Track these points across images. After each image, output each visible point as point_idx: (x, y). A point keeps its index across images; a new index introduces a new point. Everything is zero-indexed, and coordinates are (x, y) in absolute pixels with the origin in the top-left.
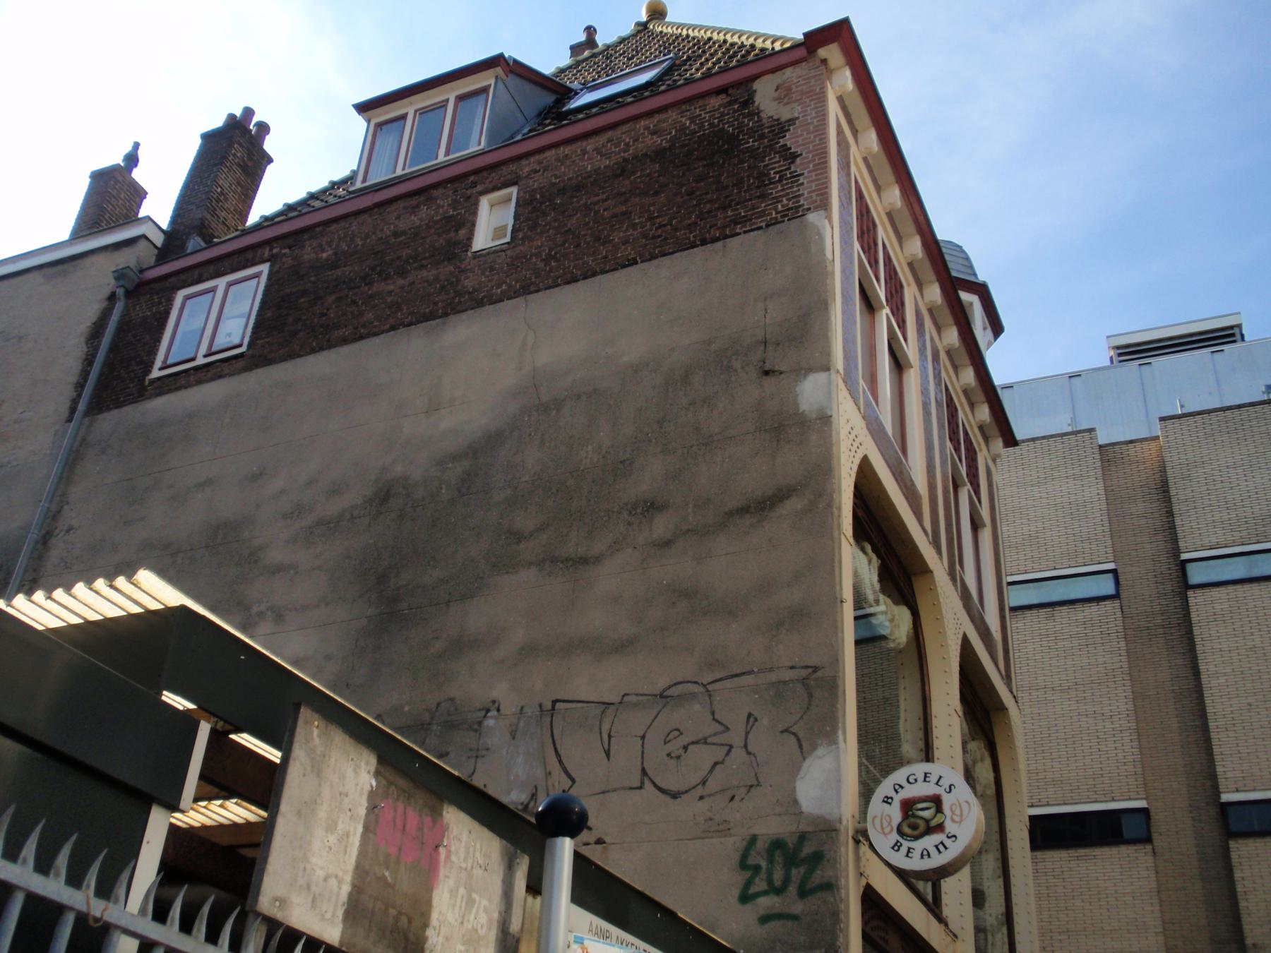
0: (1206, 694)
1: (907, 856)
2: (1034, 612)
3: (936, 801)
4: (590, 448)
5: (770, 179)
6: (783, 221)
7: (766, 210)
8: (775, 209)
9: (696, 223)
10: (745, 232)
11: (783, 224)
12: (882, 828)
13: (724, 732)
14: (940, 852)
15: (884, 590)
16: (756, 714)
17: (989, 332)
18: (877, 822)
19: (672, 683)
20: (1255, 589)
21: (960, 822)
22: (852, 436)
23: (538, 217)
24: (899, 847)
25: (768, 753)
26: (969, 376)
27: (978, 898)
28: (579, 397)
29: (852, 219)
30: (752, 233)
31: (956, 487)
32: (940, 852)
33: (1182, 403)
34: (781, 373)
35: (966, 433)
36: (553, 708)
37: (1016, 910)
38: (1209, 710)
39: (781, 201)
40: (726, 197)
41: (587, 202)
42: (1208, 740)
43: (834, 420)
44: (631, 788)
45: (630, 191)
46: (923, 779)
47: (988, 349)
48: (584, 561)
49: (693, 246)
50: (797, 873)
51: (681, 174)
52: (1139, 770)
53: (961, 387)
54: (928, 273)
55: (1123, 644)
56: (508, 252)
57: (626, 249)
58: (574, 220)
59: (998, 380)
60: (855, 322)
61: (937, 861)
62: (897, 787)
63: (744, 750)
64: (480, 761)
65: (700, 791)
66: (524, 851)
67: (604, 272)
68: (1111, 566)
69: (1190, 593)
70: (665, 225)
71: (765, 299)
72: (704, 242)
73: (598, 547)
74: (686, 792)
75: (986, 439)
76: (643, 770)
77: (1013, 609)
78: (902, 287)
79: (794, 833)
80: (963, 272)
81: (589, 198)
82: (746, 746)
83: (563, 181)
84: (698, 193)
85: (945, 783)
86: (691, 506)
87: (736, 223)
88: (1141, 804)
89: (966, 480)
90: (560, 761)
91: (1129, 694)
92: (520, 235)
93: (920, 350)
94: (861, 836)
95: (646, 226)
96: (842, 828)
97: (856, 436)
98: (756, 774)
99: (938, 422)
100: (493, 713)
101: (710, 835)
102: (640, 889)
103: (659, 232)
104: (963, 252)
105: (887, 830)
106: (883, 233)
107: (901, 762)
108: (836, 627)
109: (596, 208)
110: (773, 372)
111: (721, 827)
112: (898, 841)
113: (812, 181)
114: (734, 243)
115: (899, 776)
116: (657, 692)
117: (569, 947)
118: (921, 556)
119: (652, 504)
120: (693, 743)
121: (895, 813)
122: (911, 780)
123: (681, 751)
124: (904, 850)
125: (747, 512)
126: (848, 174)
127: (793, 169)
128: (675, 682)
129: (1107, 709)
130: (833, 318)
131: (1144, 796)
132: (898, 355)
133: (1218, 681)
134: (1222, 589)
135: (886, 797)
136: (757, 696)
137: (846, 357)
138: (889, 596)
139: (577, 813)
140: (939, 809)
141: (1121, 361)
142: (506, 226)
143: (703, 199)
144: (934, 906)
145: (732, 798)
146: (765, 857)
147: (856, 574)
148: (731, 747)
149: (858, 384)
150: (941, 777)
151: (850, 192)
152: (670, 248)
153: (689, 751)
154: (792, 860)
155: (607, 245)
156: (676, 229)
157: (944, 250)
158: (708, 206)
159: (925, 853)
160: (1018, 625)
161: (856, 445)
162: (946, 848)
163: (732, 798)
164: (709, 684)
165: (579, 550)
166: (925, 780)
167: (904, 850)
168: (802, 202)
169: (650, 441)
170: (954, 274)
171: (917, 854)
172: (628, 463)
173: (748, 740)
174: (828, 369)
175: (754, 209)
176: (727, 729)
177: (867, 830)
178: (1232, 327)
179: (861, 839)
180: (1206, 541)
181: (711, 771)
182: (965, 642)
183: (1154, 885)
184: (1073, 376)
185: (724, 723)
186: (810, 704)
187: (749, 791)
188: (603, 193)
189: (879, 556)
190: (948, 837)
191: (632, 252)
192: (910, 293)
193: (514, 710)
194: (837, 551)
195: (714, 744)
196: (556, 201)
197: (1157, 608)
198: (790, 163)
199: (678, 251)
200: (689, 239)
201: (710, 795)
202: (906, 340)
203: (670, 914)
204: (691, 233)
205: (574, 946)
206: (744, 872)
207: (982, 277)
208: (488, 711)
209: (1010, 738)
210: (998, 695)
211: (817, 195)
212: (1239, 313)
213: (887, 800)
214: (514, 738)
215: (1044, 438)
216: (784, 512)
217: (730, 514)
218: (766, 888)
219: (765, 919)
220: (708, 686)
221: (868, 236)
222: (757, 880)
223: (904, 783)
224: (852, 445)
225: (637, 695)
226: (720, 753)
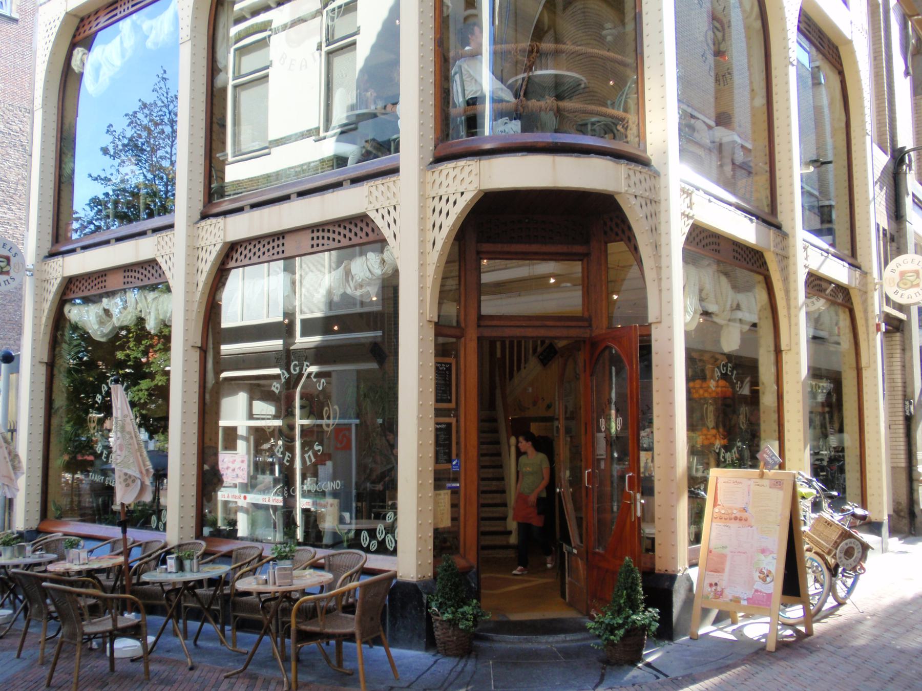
140: (8, 264)
167: (899, 294)
223: (902, 264)
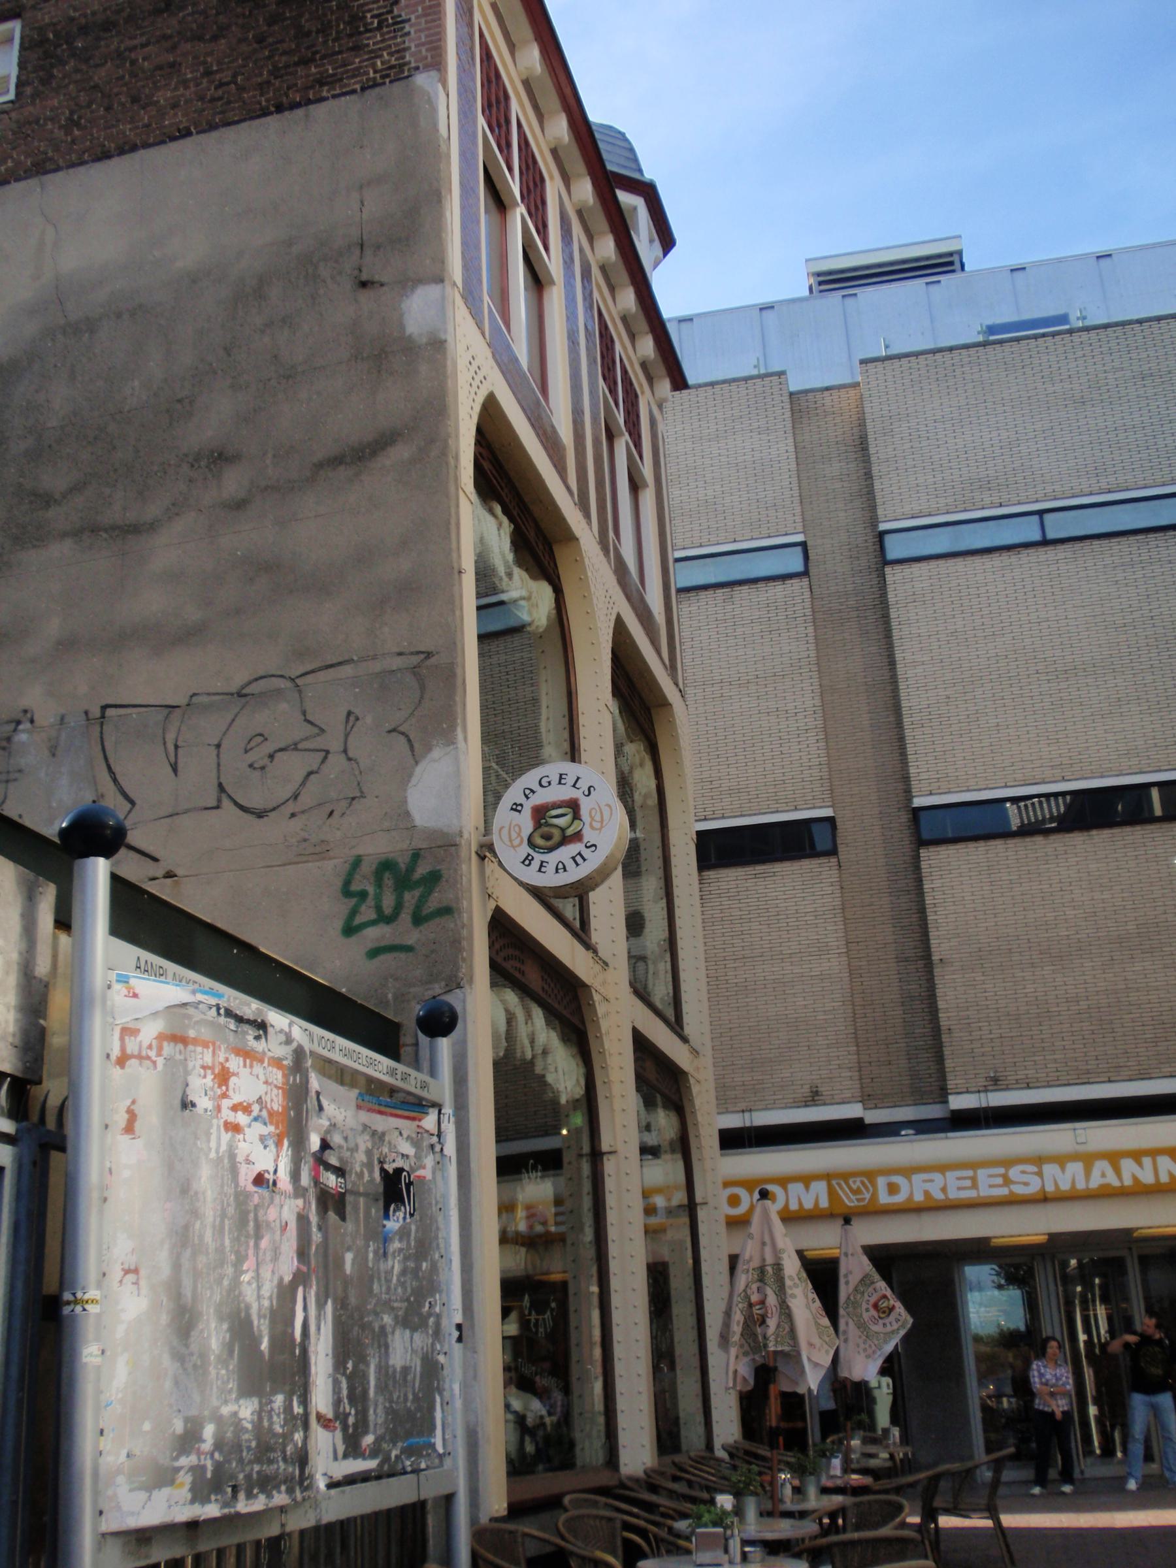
0: (902, 686)
1: (540, 870)
2: (710, 592)
3: (573, 806)
4: (136, 383)
5: (365, 25)
6: (384, 83)
7: (361, 67)
8: (374, 66)
9: (268, 82)
10: (334, 97)
11: (383, 88)
12: (511, 841)
13: (318, 735)
14: (577, 865)
15: (519, 562)
16: (357, 711)
17: (657, 248)
18: (505, 832)
19: (252, 678)
20: (959, 564)
21: (600, 829)
22: (474, 367)
23: (52, 66)
24: (530, 861)
25: (373, 758)
26: (628, 299)
27: (635, 924)
28: (119, 316)
29: (475, 84)
30: (343, 98)
31: (611, 437)
32: (577, 865)
33: (887, 343)
34: (382, 285)
35: (625, 371)
36: (103, 717)
37: (680, 934)
38: (904, 704)
39: (382, 56)
40: (308, 48)
41: (119, 47)
42: (901, 739)
43: (450, 345)
44: (206, 809)
45: (179, 33)
46: (557, 781)
47: (655, 267)
48: (135, 529)
49: (265, 113)
50: (410, 898)
51: (247, 13)
52: (825, 775)
53: (619, 313)
54: (577, 165)
55: (811, 630)
56: (13, 115)
57: (176, 115)
58: (102, 72)
59: (668, 310)
60: (478, 222)
61: (575, 874)
62: (527, 792)
63: (343, 755)
64: (11, 786)
65: (291, 807)
66: (50, 878)
67: (146, 145)
68: (800, 538)
69: (888, 570)
70: (228, 84)
71: (361, 187)
72: (280, 109)
73: (153, 510)
74: (274, 809)
75: (650, 379)
76: (220, 785)
77: (680, 591)
78: (542, 180)
79: (407, 850)
80: (625, 167)
81: (122, 41)
82: (345, 751)
83: (85, 16)
84: (271, 40)
85: (583, 785)
86: (270, 455)
87: (322, 84)
88: (827, 812)
89: (624, 429)
90: (115, 780)
91: (816, 687)
92: (28, 90)
93: (565, 262)
94: (486, 851)
95: (201, 83)
96: (463, 842)
97: (479, 368)
98: (359, 784)
99: (588, 355)
100: (26, 725)
101: (305, 858)
102: (209, 921)
103: (220, 92)
104: (626, 140)
105: (516, 842)
106: (519, 107)
107: (536, 761)
108: (453, 603)
109: (133, 55)
110: (373, 283)
111: (318, 849)
112: (529, 855)
113: (420, 31)
114: (319, 111)
115: (530, 779)
116: (234, 690)
117: (109, 987)
118: (564, 519)
119: (220, 455)
120: (281, 750)
121: (526, 823)
122: (544, 783)
123: (266, 761)
124: (536, 864)
125: (341, 463)
126: (470, 24)
127: (396, 12)
128: (255, 677)
129: (790, 706)
130: (448, 214)
131: (830, 804)
132: (537, 268)
133: (915, 671)
134: (923, 566)
135: (515, 804)
136: (357, 690)
137: (466, 267)
138: (527, 570)
139: (111, 827)
140: (576, 816)
141: (821, 291)
142: (8, 77)
143: (277, 49)
144: (581, 932)
145: (331, 813)
146: (372, 881)
147: (481, 541)
148: (327, 752)
149: (482, 301)
150: (578, 778)
151: (472, 49)
152: (235, 115)
153: (276, 760)
154: (404, 882)
155: (148, 109)
156: (241, 89)
157: (597, 136)
158: (284, 58)
159: (561, 866)
160: (689, 612)
161: (478, 378)
162: (584, 860)
163: (331, 813)
164: (297, 677)
165: (128, 514)
166: (560, 783)
167: (536, 864)
168: (408, 58)
169: (215, 373)
170: (610, 167)
171: (550, 868)
172: (187, 401)
173: (348, 743)
174: (442, 281)
175: (345, 65)
176: (322, 730)
177: (493, 844)
178: (951, 254)
179: (488, 854)
180: (907, 509)
181: (303, 784)
182: (620, 628)
183: (838, 902)
184: (765, 308)
185: (317, 723)
186: (422, 697)
187: (350, 804)
188: (142, 35)
189: (511, 519)
190: (587, 847)
191: (184, 120)
192: (553, 188)
193: (52, 720)
194: (453, 510)
195: (306, 750)
196: (76, 44)
197: (850, 587)
198: (392, 5)
199: (244, 120)
200: (260, 104)
201: (303, 812)
202: (547, 248)
203: (249, 949)
204: (262, 95)
205: (117, 987)
206: (346, 900)
207: (649, 175)
208: (18, 723)
209: (675, 737)
210: (661, 690)
211: (427, 50)
212: (960, 237)
213: (516, 808)
214: (54, 755)
215: (724, 382)
216: (388, 463)
217: (319, 466)
218: (373, 916)
219: (374, 953)
220: (297, 681)
221: (498, 108)
222: (363, 908)
223: (536, 787)
224: (473, 378)
225: (209, 694)
226: (314, 760)
